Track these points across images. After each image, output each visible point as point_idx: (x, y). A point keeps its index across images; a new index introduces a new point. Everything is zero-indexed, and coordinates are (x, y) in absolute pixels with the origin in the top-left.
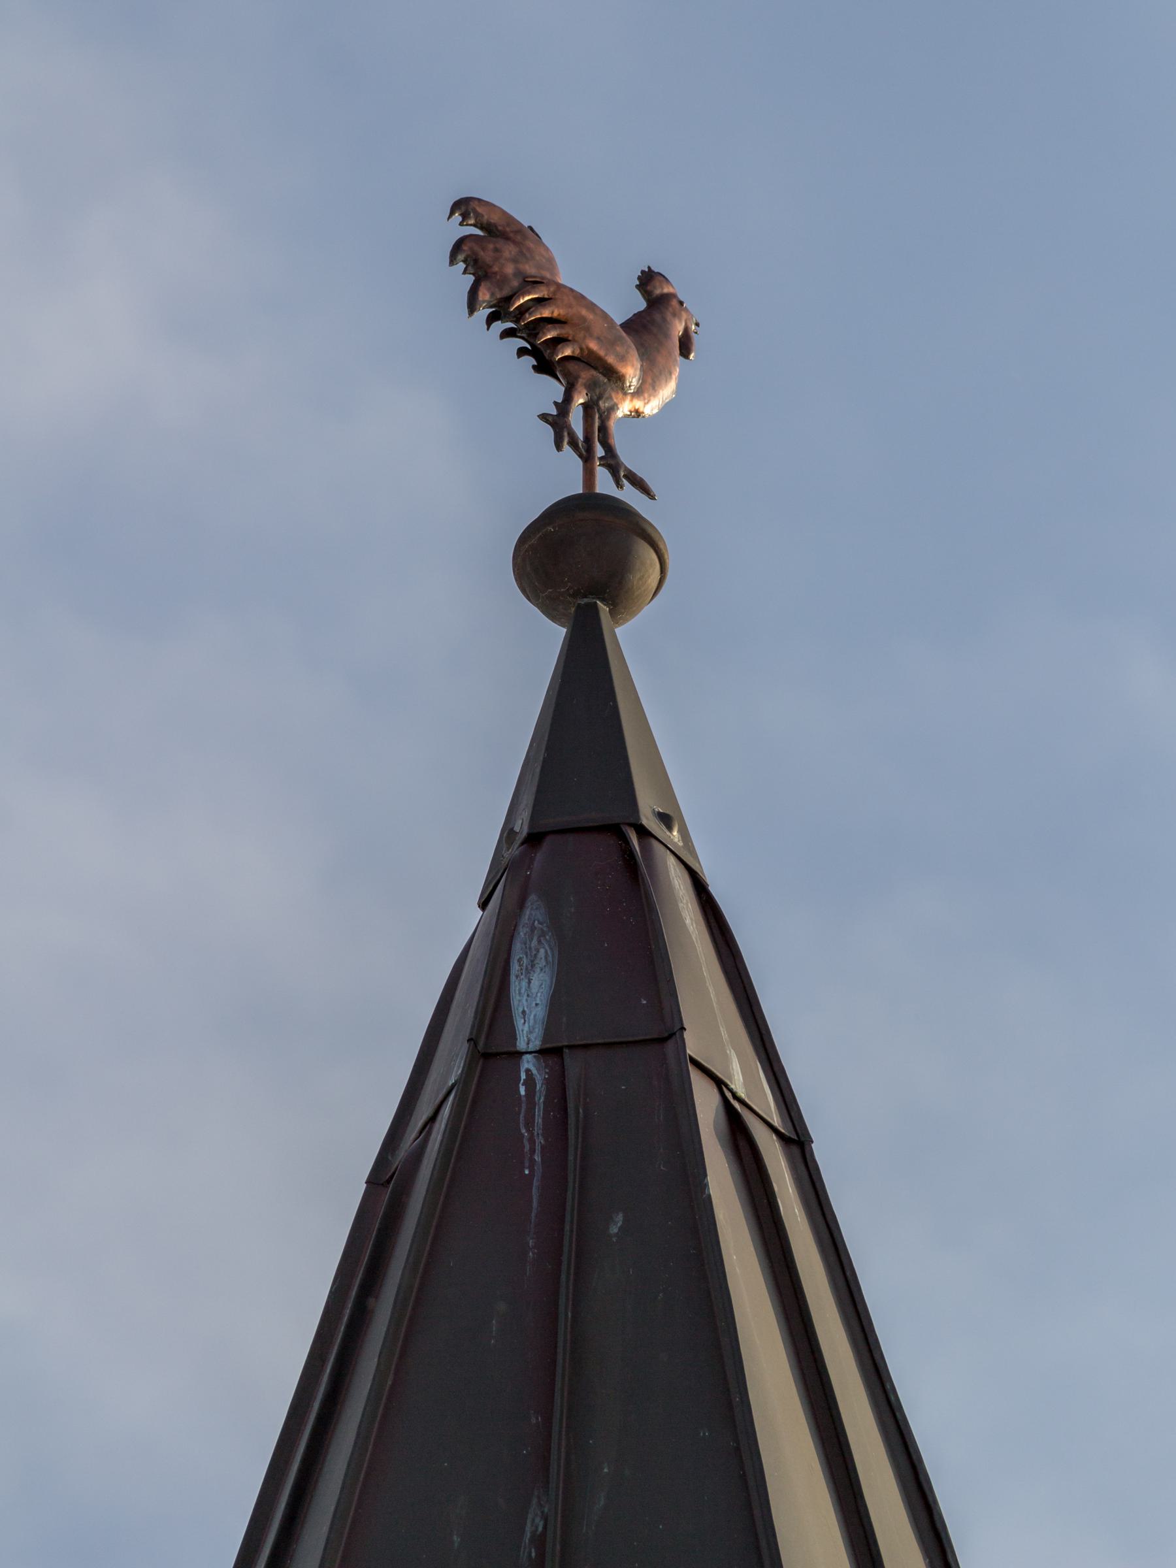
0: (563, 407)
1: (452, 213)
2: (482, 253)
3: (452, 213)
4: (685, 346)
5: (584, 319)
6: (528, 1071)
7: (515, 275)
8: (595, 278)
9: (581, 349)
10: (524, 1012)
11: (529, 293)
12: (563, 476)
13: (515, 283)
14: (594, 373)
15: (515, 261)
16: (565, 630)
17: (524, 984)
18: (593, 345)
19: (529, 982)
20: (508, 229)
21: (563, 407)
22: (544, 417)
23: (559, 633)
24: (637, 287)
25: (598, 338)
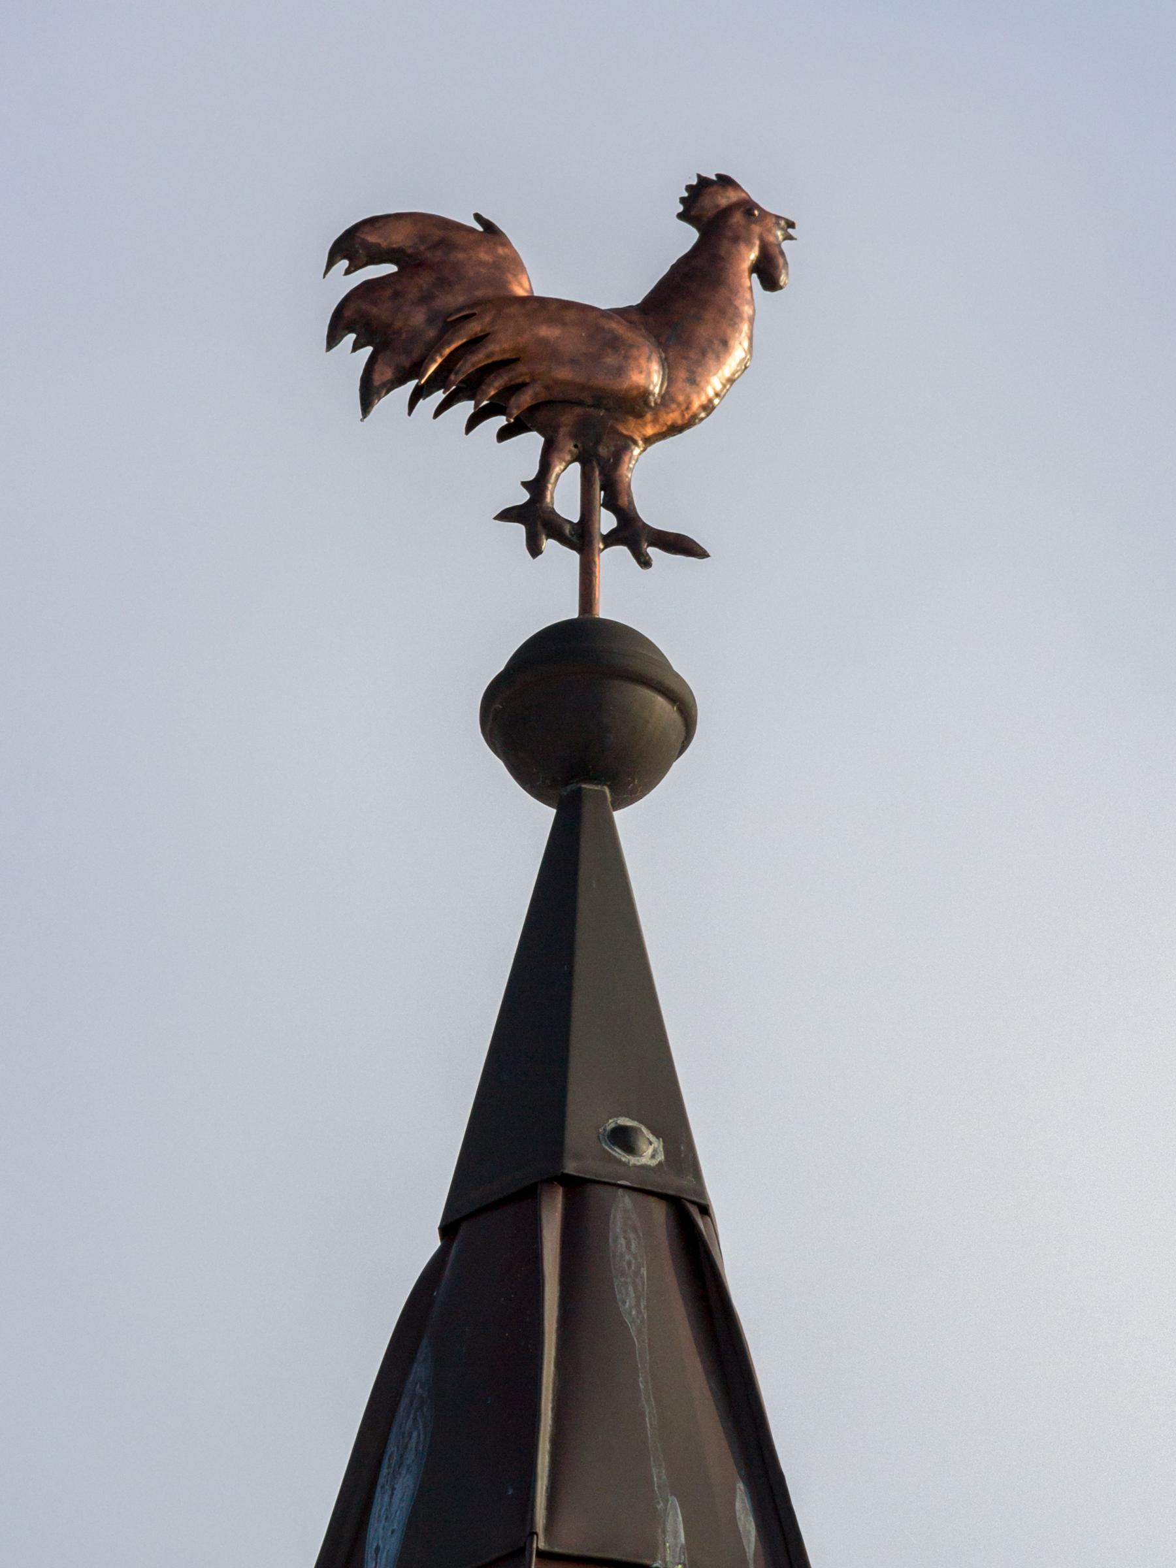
0: (537, 486)
1: (330, 264)
2: (375, 310)
3: (330, 264)
4: (768, 272)
5: (543, 342)
6: (626, 1211)
7: (430, 321)
8: (591, 250)
9: (547, 387)
10: (378, 1548)
11: (449, 343)
12: (544, 589)
13: (431, 333)
14: (578, 410)
15: (426, 298)
16: (554, 811)
17: (387, 1498)
18: (564, 373)
19: (392, 1494)
20: (422, 248)
21: (537, 486)
22: (507, 515)
23: (549, 814)
24: (681, 216)
25: (573, 361)
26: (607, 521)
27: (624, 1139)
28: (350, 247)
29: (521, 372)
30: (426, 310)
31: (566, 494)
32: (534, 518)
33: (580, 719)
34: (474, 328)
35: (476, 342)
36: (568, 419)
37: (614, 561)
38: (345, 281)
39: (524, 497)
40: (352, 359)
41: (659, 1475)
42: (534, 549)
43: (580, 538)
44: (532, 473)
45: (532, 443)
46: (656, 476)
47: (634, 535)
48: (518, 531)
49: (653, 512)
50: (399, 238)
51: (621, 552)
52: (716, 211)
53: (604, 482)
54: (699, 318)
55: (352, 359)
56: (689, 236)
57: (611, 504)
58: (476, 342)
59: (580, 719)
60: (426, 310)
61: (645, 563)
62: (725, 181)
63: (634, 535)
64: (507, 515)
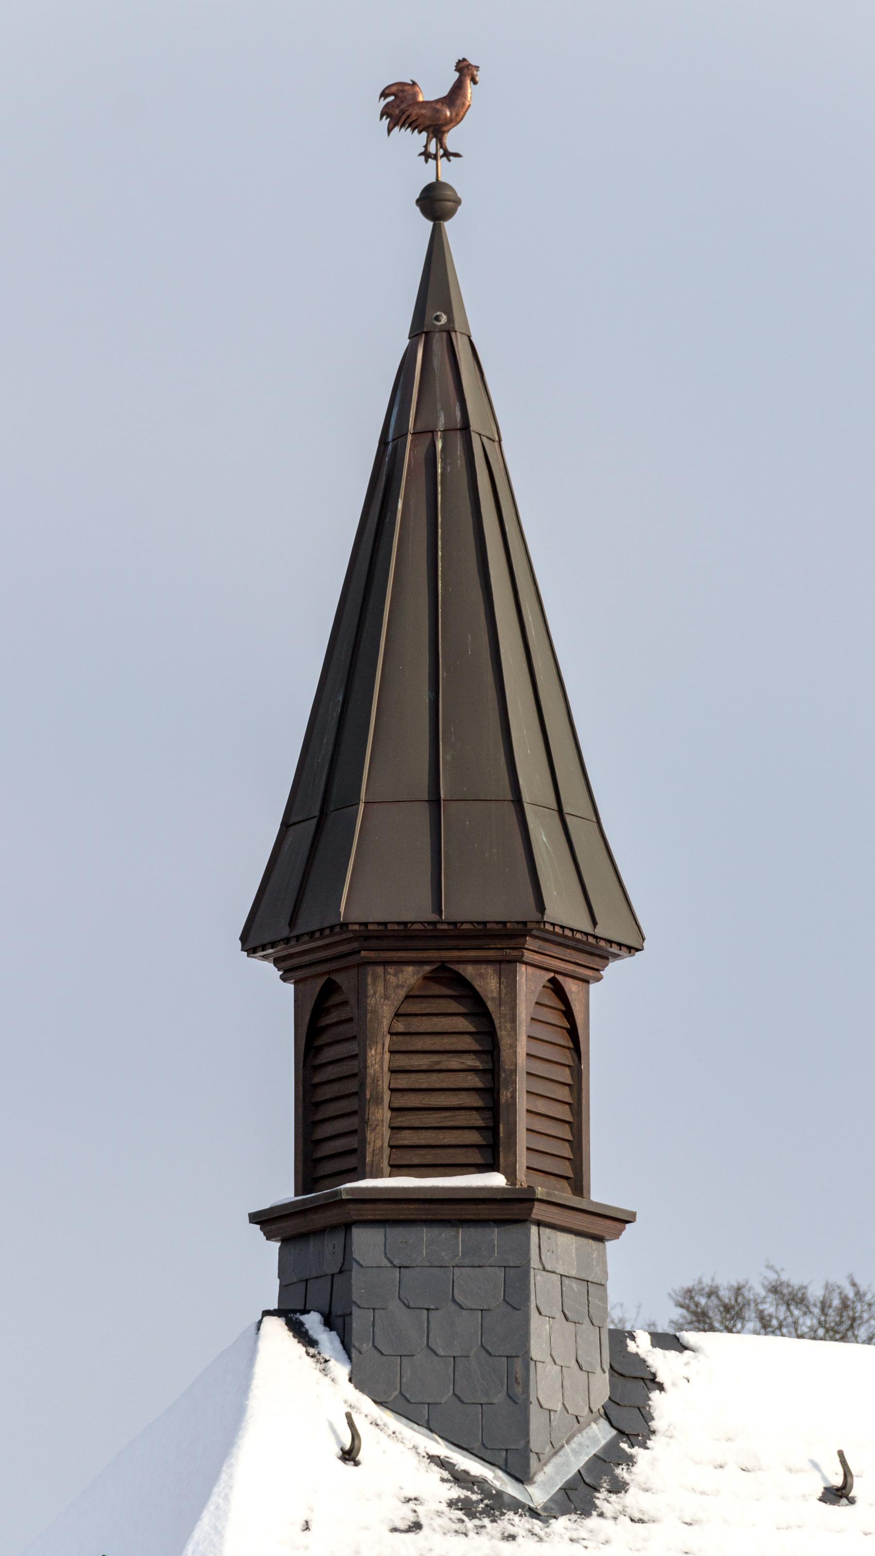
0: (426, 146)
8: (433, 89)
12: (425, 174)
22: (421, 154)
23: (431, 224)
26: (441, 152)
27: (437, 318)
28: (384, 95)
29: (419, 122)
30: (402, 108)
31: (432, 149)
32: (426, 155)
33: (435, 203)
34: (408, 113)
35: (408, 117)
36: (431, 130)
37: (443, 161)
38: (383, 102)
39: (423, 150)
40: (386, 122)
41: (439, 406)
42: (426, 161)
43: (435, 157)
44: (424, 144)
45: (424, 134)
46: (453, 139)
47: (447, 154)
48: (423, 157)
49: (451, 149)
50: (394, 89)
51: (445, 159)
52: (464, 69)
53: (441, 143)
54: (457, 99)
55: (386, 122)
56: (457, 75)
57: (441, 147)
58: (408, 117)
59: (435, 203)
60: (402, 108)
61: (449, 160)
62: (464, 60)
63: (447, 154)
64: (421, 154)
